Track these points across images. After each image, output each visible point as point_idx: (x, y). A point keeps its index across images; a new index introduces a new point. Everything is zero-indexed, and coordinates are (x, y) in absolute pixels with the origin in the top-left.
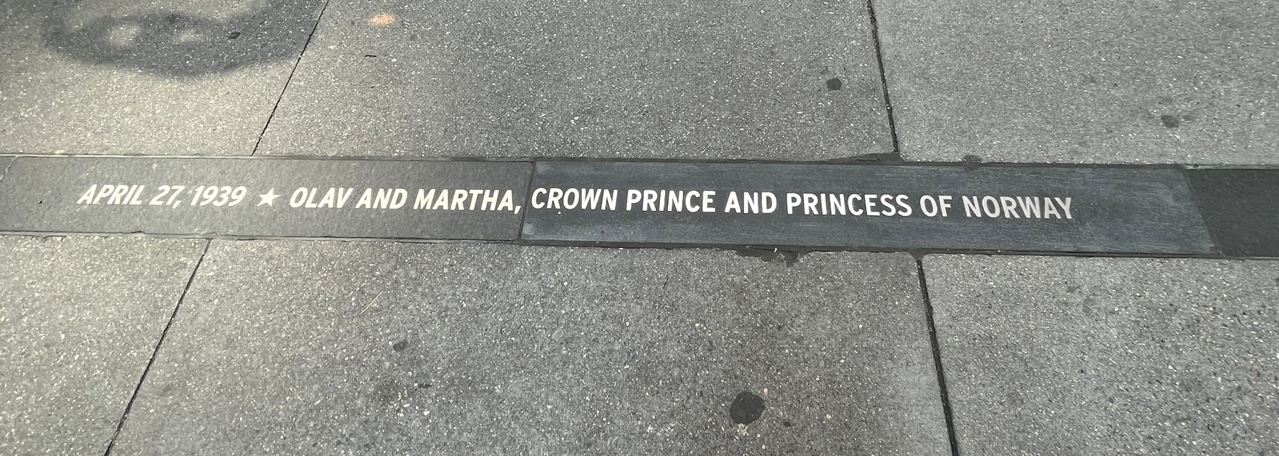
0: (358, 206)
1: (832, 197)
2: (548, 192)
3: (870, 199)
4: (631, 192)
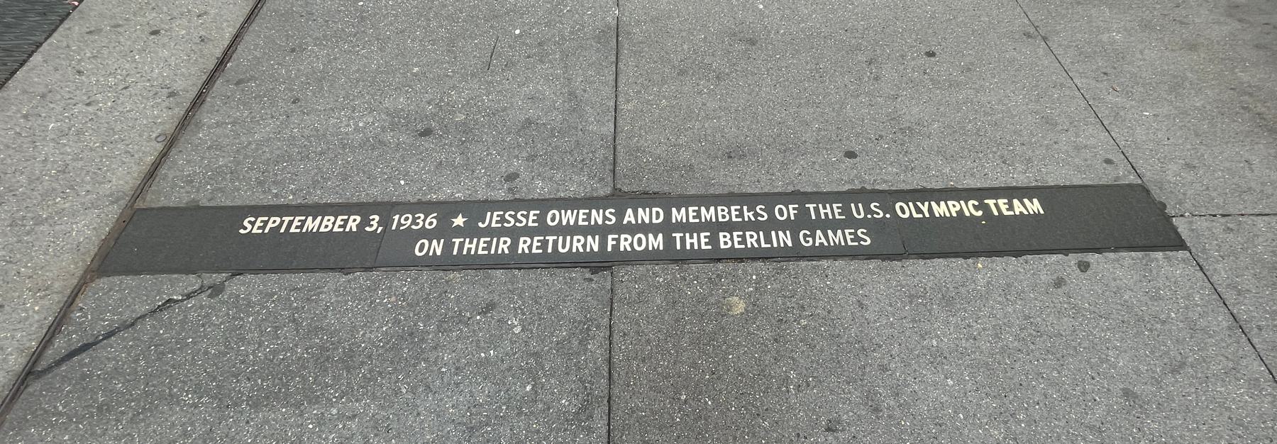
4: (721, 234)
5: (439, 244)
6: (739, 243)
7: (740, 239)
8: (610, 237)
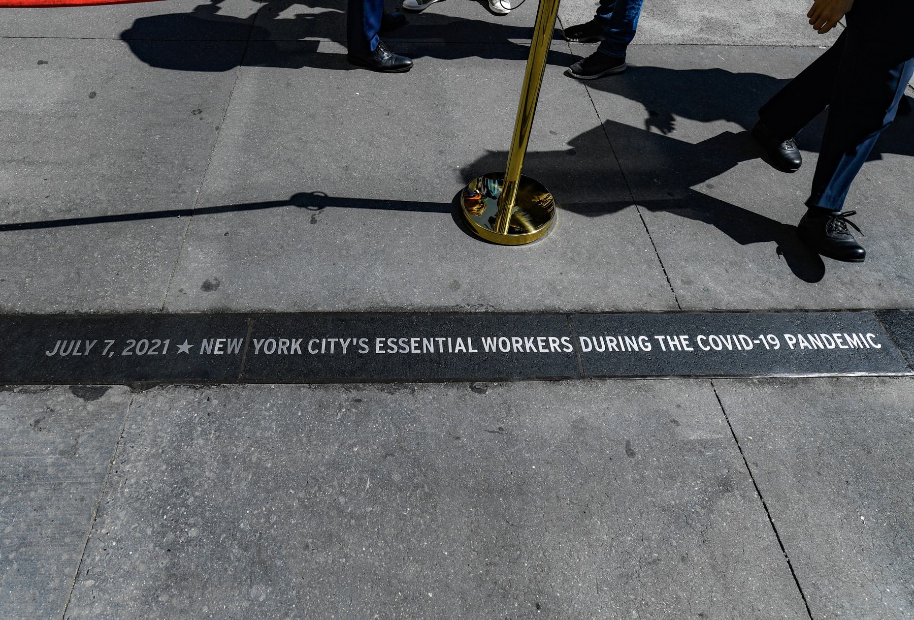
1: (626, 338)
2: (753, 343)
3: (541, 340)
5: (205, 350)
7: (417, 345)
8: (378, 340)
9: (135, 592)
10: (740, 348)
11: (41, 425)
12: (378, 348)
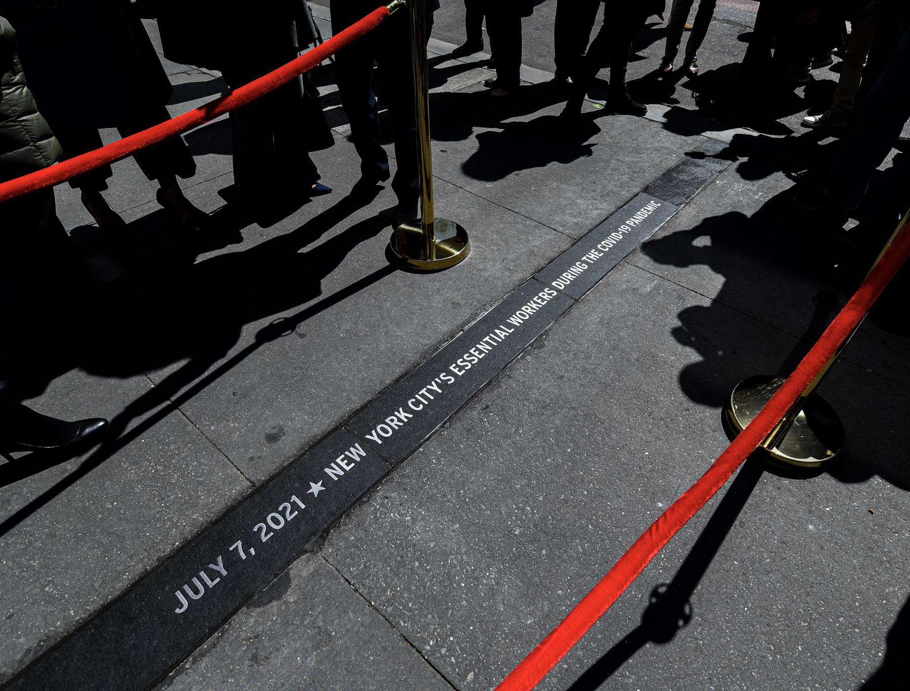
0: (220, 558)
6: (480, 354)
9: (507, 640)
10: (619, 240)
11: (262, 654)
12: (458, 373)
